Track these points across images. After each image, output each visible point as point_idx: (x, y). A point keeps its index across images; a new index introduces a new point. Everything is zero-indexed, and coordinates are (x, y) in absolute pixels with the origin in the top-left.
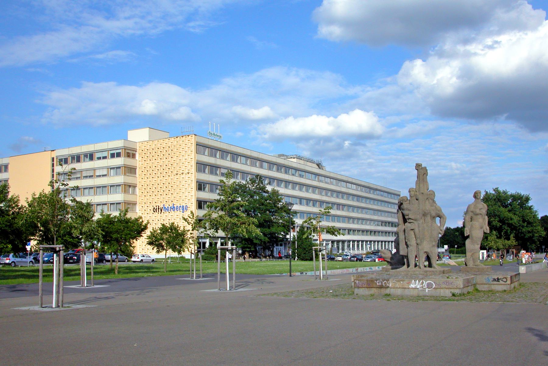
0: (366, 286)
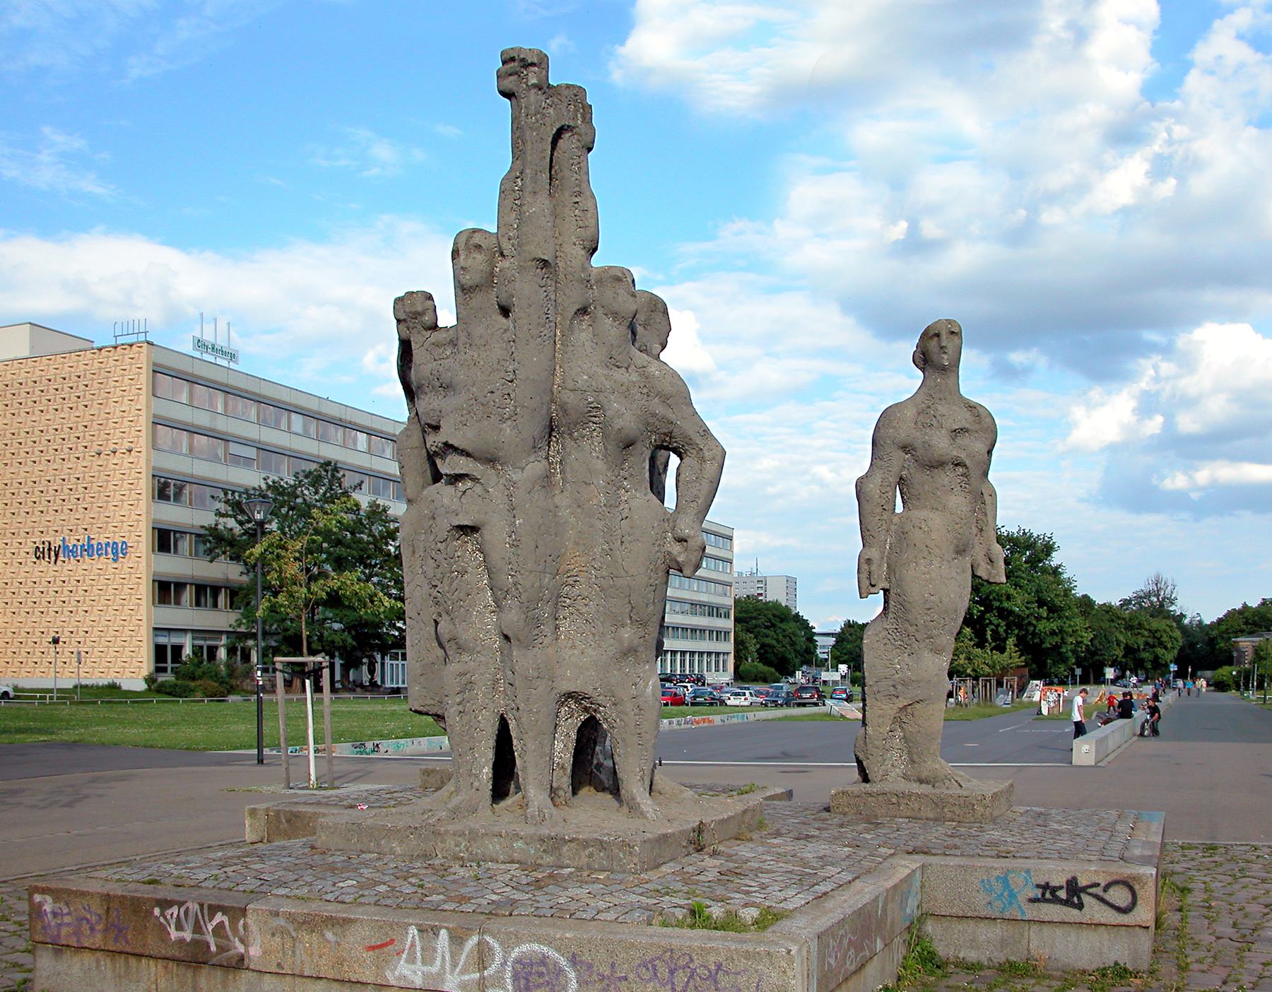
0: (98, 940)
